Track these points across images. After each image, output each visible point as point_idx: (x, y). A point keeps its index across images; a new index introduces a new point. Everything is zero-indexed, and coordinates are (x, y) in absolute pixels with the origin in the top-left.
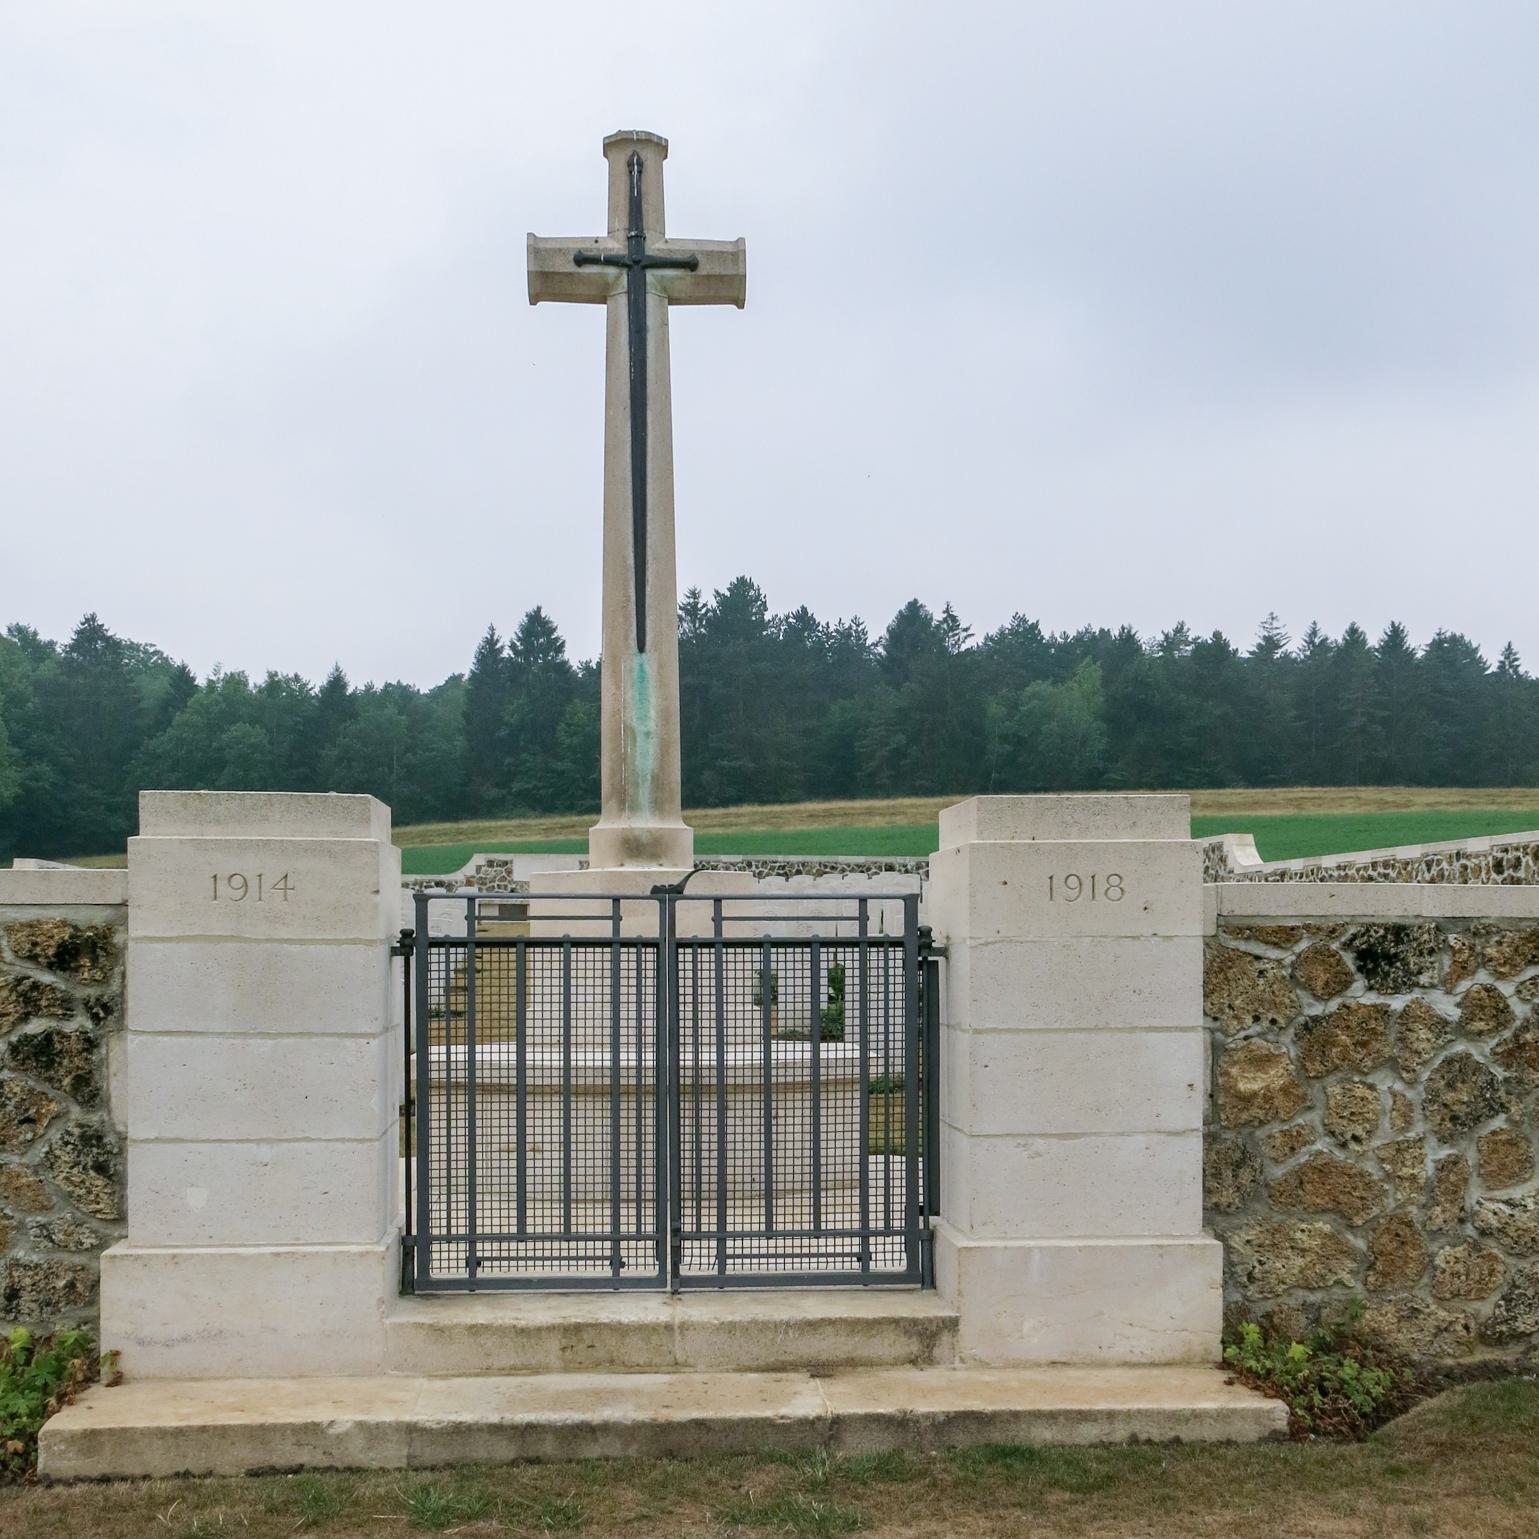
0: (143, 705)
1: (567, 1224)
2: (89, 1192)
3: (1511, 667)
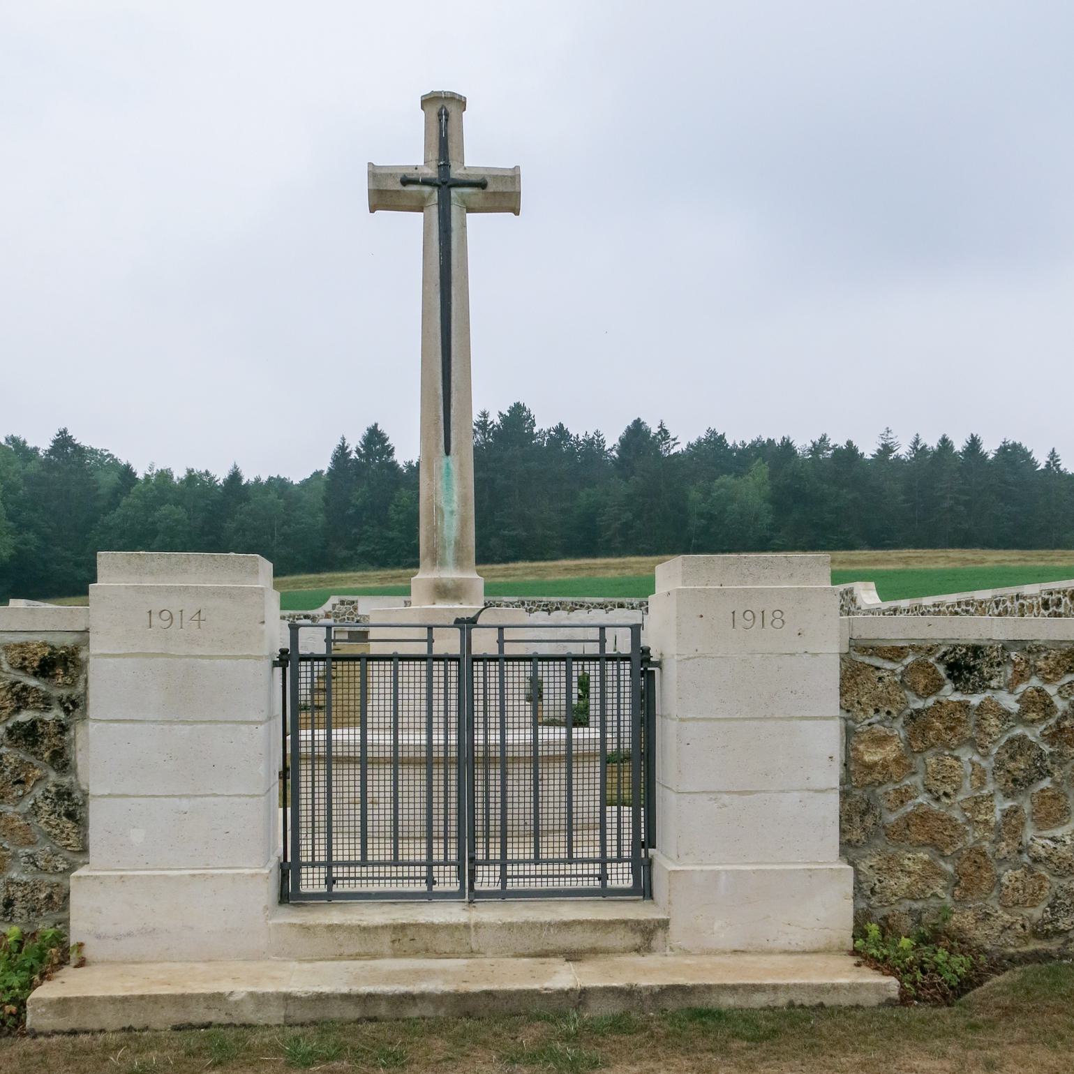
0: (100, 492)
1: (396, 854)
2: (62, 832)
3: (1054, 465)
